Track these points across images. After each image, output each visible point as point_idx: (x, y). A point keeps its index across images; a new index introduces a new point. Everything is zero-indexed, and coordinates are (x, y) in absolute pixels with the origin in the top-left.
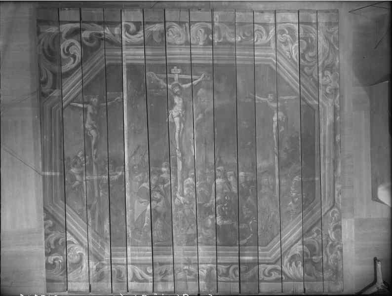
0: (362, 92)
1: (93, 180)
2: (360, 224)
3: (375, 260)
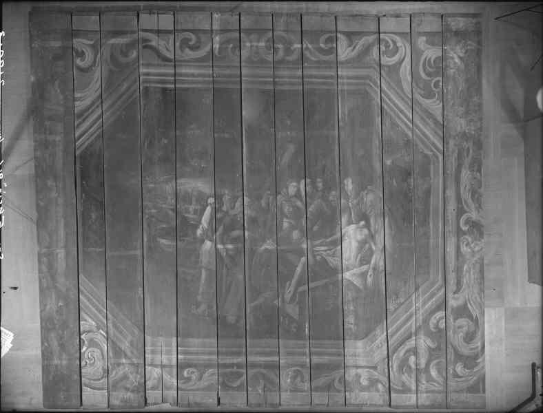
0: (512, 131)
1: (171, 355)
2: (513, 315)
3: (534, 365)
